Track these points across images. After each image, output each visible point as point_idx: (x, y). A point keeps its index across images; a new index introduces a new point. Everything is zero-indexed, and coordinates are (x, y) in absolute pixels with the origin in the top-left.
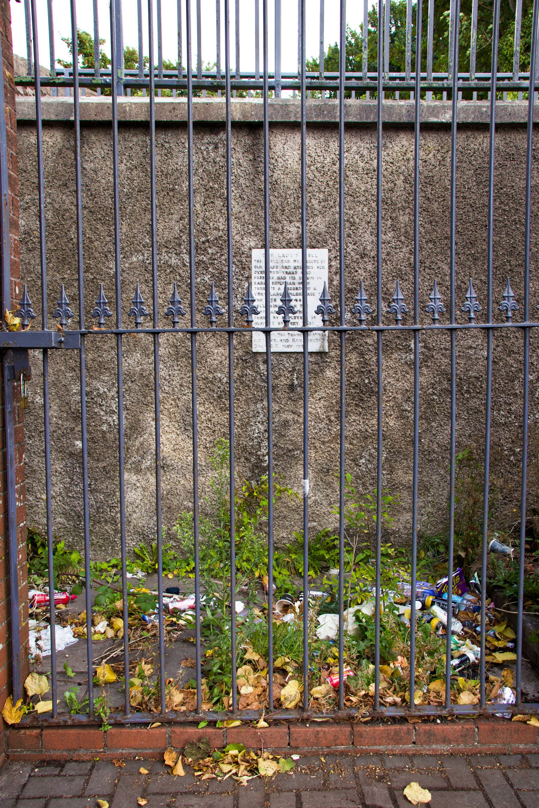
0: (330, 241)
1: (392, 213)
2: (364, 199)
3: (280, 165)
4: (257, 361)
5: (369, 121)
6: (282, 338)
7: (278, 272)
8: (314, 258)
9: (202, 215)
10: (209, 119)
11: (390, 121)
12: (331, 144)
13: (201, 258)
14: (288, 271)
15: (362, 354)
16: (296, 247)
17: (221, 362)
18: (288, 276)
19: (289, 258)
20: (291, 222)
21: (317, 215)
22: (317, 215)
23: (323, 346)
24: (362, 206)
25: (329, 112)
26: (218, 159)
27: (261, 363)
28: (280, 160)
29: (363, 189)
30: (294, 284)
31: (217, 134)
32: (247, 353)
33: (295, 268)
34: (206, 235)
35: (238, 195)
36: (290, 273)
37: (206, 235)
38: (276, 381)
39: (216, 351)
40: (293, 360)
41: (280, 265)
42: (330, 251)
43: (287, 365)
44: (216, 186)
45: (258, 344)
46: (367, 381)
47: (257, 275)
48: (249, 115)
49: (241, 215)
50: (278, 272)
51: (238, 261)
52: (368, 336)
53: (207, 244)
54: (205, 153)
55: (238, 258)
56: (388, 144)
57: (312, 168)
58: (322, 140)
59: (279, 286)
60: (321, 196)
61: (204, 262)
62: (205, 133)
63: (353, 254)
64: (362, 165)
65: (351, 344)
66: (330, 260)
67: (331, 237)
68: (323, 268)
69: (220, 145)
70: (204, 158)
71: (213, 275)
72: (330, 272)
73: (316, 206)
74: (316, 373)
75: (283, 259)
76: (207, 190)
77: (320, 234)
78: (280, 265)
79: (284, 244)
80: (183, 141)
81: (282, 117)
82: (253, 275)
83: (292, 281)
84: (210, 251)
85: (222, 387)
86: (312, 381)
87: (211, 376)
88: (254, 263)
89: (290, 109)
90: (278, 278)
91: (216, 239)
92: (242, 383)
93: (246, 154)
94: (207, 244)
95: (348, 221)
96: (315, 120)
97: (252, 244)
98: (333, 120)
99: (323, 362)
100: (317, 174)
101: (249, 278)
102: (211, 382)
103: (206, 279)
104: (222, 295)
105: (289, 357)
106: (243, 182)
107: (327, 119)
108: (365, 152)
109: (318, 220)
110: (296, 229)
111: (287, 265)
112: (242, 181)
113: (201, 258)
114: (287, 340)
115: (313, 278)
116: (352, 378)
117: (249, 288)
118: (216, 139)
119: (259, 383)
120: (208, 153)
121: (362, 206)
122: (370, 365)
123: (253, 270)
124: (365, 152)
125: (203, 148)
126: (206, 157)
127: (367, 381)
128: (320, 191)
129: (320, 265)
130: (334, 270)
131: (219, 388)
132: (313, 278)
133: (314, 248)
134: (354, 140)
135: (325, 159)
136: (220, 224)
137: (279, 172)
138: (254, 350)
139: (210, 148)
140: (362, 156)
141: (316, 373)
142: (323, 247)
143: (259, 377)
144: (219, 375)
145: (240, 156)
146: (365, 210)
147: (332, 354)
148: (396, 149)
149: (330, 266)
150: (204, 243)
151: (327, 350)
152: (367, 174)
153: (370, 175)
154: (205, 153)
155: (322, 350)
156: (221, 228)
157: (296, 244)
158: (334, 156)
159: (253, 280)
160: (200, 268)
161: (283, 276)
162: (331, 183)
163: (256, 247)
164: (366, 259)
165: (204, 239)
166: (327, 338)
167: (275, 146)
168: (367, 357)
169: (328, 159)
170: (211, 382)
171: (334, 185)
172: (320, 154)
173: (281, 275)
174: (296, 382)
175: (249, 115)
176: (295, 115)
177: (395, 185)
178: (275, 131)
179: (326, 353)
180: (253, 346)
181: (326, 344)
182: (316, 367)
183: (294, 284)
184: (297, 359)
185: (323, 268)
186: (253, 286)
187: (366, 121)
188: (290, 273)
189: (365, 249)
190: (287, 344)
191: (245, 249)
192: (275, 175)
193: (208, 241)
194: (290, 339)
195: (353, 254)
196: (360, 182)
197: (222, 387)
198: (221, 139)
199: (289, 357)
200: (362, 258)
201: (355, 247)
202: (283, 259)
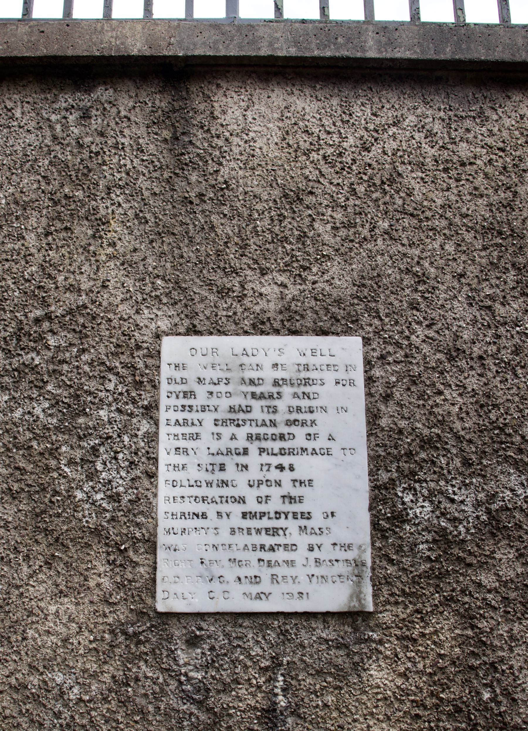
0: (365, 319)
1: (515, 254)
2: (444, 223)
3: (236, 150)
4: (170, 639)
5: (442, 57)
6: (243, 572)
7: (229, 394)
8: (326, 360)
9: (39, 257)
10: (70, 53)
11: (490, 58)
12: (356, 109)
13: (27, 358)
14: (258, 390)
15: (468, 618)
16: (277, 332)
17: (65, 640)
18: (256, 405)
19: (260, 358)
20: (263, 272)
21: (329, 258)
22: (329, 258)
23: (358, 595)
24: (440, 239)
25: (349, 40)
26: (89, 139)
27: (181, 644)
28: (235, 140)
29: (439, 202)
30: (273, 423)
31: (88, 91)
32: (141, 614)
33: (276, 383)
34: (45, 303)
35: (131, 213)
36: (262, 396)
37: (45, 303)
38: (225, 698)
39: (53, 609)
40: (272, 636)
41: (235, 375)
42: (367, 341)
43: (256, 651)
44: (79, 194)
45: (173, 588)
46: (486, 696)
47: (173, 401)
48: (163, 44)
49: (136, 257)
50: (229, 394)
51: (125, 366)
52: (481, 565)
53: (46, 325)
54: (58, 127)
55: (124, 358)
56: (488, 112)
57: (314, 156)
58: (335, 102)
59: (233, 429)
60: (339, 216)
61: (33, 369)
62: (62, 90)
63: (426, 349)
64: (432, 152)
65: (438, 589)
66: (368, 363)
67: (368, 310)
68: (352, 383)
69: (94, 112)
70: (55, 138)
71: (56, 402)
72: (369, 395)
73: (327, 238)
74: (340, 674)
75: (245, 360)
76: (56, 203)
77: (338, 302)
78: (235, 375)
79: (247, 324)
80: (10, 105)
81: (241, 47)
82: (164, 402)
83: (267, 417)
84: (52, 341)
85: (67, 714)
86: (330, 699)
87: (35, 679)
88: (166, 372)
89: (260, 33)
90: (232, 409)
91: (70, 312)
92: (123, 703)
93: (155, 129)
94: (46, 325)
95: (408, 271)
96: (316, 53)
97: (164, 324)
98: (359, 55)
99: (359, 641)
100: (326, 169)
101: (150, 410)
102: (36, 698)
103: (38, 411)
104: (78, 454)
105: (263, 628)
106: (147, 184)
107: (345, 53)
108: (437, 127)
109: (334, 268)
110: (276, 289)
111: (254, 375)
112: (143, 183)
113: (27, 358)
114: (256, 579)
115: (324, 409)
116: (445, 687)
117: (152, 438)
118: (86, 100)
119: (174, 702)
120: (65, 127)
121: (440, 239)
122: (494, 649)
123: (164, 388)
124: (437, 127)
125: (53, 118)
126: (60, 134)
127: (486, 696)
128: (335, 205)
129: (341, 375)
130: (379, 388)
131: (58, 715)
132: (324, 409)
133: (325, 333)
134: (410, 103)
135: (344, 139)
136: (83, 278)
137: (233, 164)
138: (161, 607)
139: (71, 118)
140: (430, 134)
141: (340, 674)
142: (347, 332)
143: (173, 685)
144: (59, 678)
145: (142, 131)
146: (450, 247)
147: (386, 617)
148: (507, 122)
149: (369, 380)
150: (37, 321)
151: (371, 608)
152: (446, 170)
153: (453, 173)
154: (58, 127)
155: (355, 605)
156: (83, 287)
157: (277, 325)
158: (362, 132)
159: (163, 415)
160: (24, 385)
161: (244, 403)
162: (361, 189)
163: (174, 332)
164: (462, 363)
165: (39, 313)
166: (368, 573)
167: (224, 112)
168: (483, 624)
169: (351, 140)
170: (36, 698)
171: (368, 193)
172: (333, 129)
173: (237, 401)
174: (282, 701)
175: (163, 44)
176: (271, 44)
177: (515, 194)
178: (224, 84)
179: (366, 616)
180: (159, 595)
181: (368, 590)
182: (339, 657)
183: (273, 423)
184: (284, 633)
185: (352, 383)
186: (163, 430)
187: (435, 57)
188: (262, 396)
189: (457, 337)
190: (255, 589)
191: (145, 337)
192: (225, 171)
193: (48, 317)
194: (265, 573)
195: (426, 349)
196: (432, 187)
197: (67, 714)
198: (97, 100)
199: (263, 628)
200: (451, 359)
201: (432, 334)
202: (245, 360)
